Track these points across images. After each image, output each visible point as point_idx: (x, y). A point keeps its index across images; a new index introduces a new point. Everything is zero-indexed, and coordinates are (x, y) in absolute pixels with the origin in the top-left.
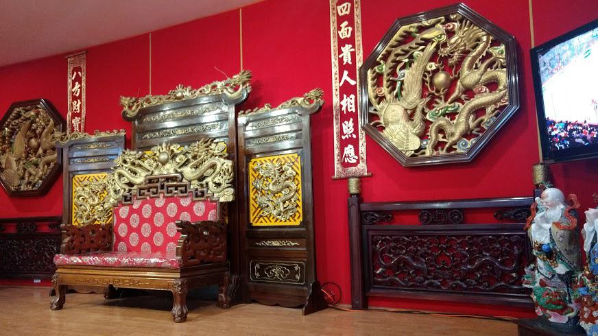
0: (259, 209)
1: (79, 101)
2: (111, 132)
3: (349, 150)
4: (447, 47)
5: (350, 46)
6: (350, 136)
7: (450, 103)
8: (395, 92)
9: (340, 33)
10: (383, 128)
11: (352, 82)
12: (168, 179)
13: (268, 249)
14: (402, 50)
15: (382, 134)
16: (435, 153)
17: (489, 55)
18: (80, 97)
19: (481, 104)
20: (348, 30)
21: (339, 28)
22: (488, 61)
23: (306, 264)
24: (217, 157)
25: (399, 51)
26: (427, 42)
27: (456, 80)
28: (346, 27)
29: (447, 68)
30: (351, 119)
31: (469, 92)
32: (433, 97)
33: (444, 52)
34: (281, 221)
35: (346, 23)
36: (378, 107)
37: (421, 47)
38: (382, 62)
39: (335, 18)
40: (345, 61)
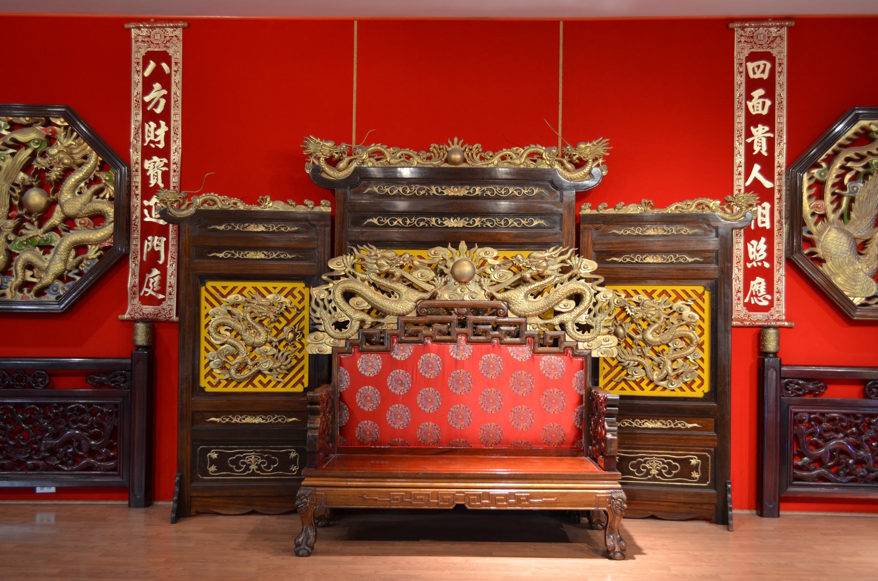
0: (620, 368)
1: (162, 123)
2: (300, 202)
3: (759, 285)
4: (45, 157)
5: (767, 129)
6: (760, 264)
7: (46, 232)
8: (841, 211)
9: (750, 104)
10: (821, 261)
11: (768, 184)
12: (477, 310)
13: (685, 433)
14: (857, 154)
15: (821, 268)
16: (20, 295)
17: (97, 180)
18: (166, 116)
19: (84, 241)
20: (764, 103)
21: (749, 98)
22: (95, 187)
23: (714, 458)
24: (583, 281)
25: (851, 154)
26: (18, 145)
27: (55, 202)
28: (760, 97)
29: (43, 185)
30: (763, 240)
31: (69, 222)
32: (22, 220)
33: (40, 163)
34: (665, 389)
35: (760, 92)
36: (814, 229)
37: (11, 151)
38: (824, 165)
39: (743, 79)
40: (757, 149)
